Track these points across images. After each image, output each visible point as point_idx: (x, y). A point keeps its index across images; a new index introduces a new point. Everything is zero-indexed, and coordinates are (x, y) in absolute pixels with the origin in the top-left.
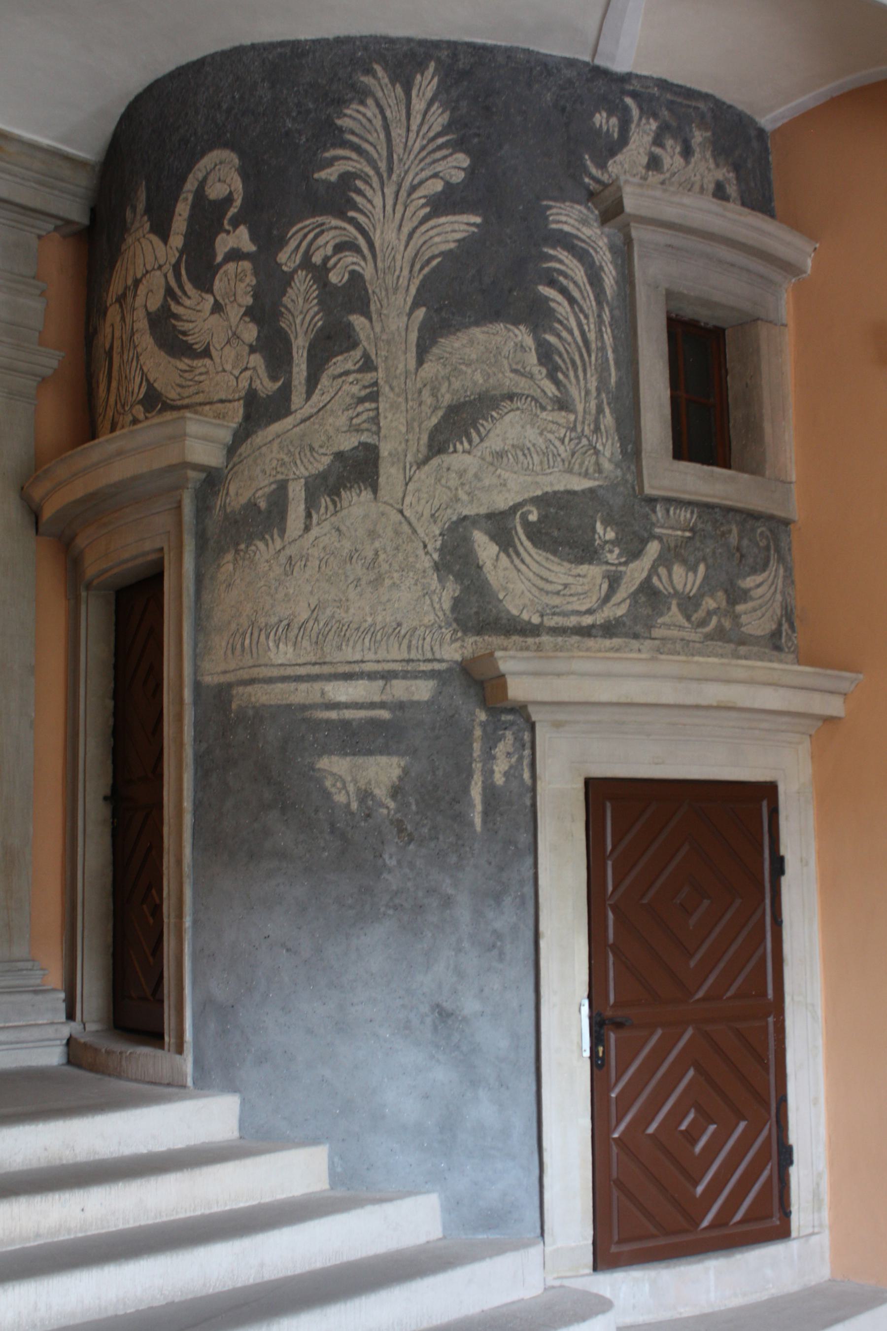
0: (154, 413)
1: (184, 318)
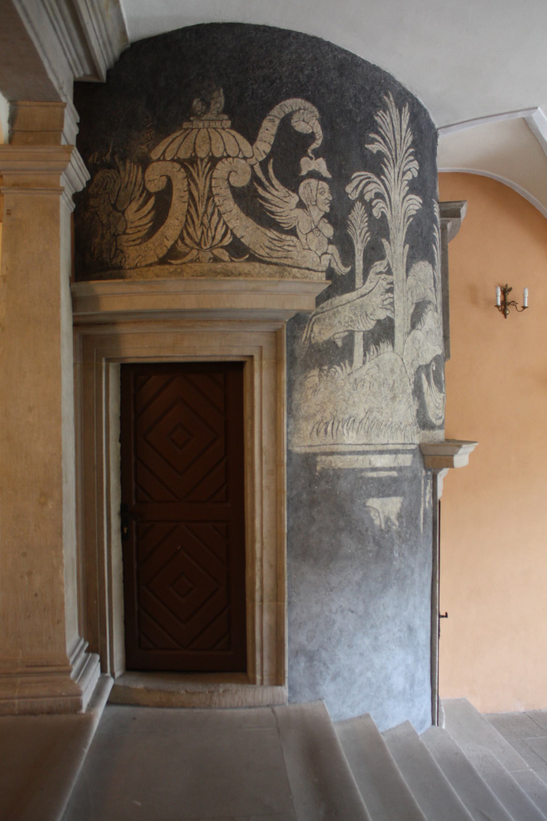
0: (242, 259)
1: (272, 202)
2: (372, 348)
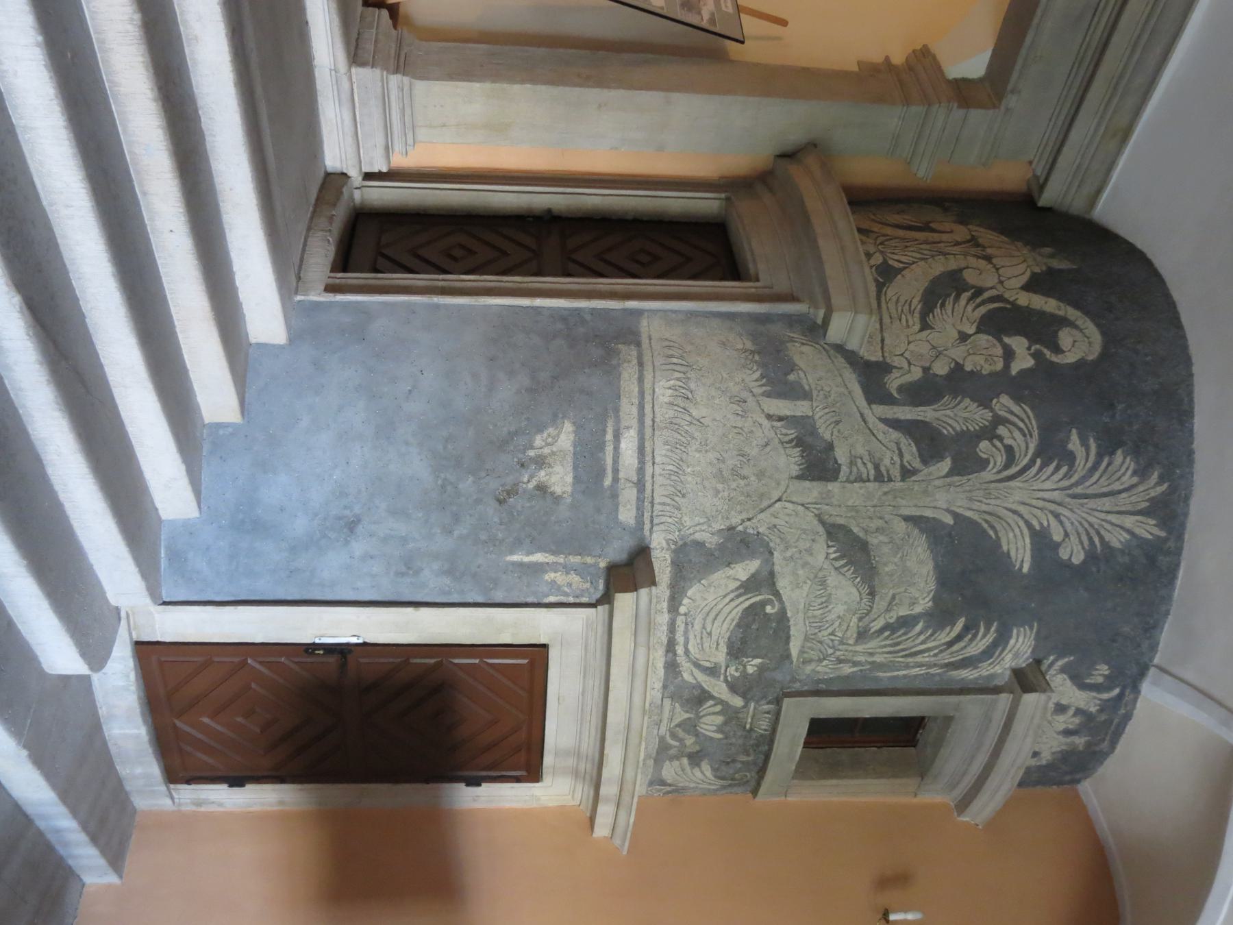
2: (792, 433)
